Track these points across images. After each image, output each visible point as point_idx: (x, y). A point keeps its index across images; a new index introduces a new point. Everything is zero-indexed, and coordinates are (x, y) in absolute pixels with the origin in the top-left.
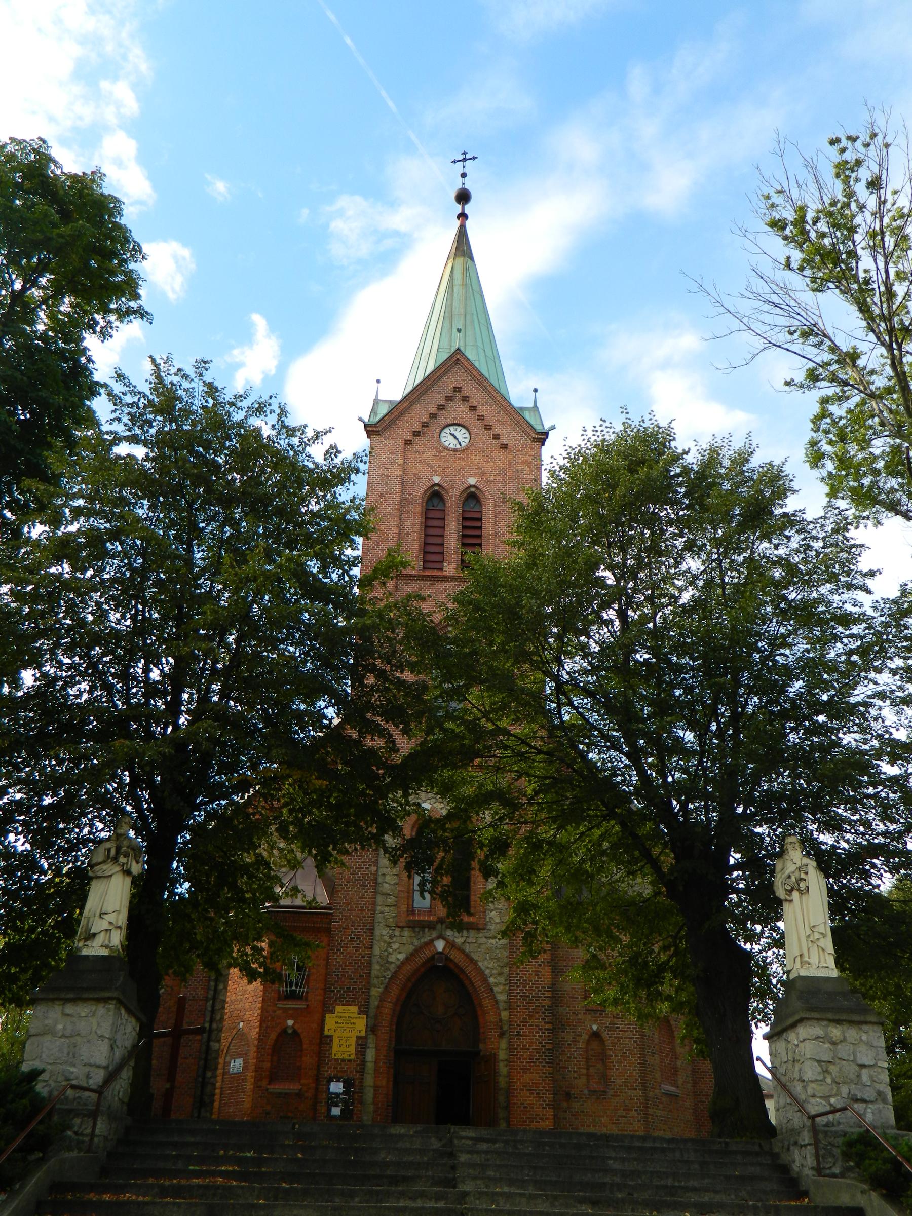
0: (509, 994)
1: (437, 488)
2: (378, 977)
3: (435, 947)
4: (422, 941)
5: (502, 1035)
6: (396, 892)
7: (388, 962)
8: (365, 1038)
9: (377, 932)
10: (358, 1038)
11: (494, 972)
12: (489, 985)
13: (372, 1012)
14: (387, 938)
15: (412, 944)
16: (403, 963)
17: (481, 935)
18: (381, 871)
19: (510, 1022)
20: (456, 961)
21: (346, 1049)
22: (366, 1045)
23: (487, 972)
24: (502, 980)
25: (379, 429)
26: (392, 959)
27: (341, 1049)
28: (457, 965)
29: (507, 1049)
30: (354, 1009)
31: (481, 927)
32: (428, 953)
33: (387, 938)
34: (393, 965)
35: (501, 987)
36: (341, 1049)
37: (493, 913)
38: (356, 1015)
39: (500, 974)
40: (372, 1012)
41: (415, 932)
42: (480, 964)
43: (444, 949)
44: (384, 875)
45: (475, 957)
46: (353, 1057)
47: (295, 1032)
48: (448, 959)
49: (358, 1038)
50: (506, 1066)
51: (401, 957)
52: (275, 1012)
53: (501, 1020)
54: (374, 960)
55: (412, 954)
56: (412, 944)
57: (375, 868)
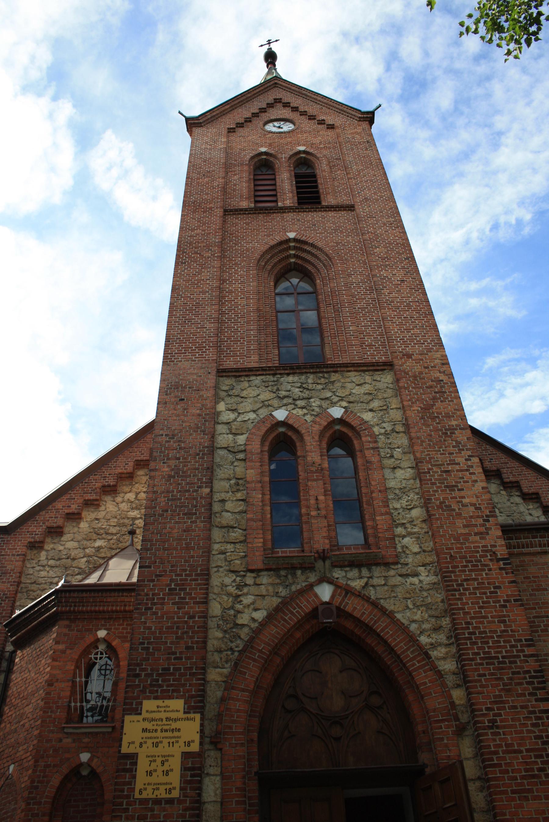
0: (460, 658)
1: (282, 430)
2: (220, 651)
3: (316, 596)
4: (294, 588)
5: (460, 731)
6: (244, 522)
7: (236, 625)
8: (200, 755)
9: (215, 581)
10: (186, 755)
11: (426, 626)
12: (420, 647)
13: (211, 709)
14: (232, 590)
15: (277, 594)
16: (263, 624)
17: (392, 573)
18: (217, 497)
19: (471, 705)
20: (357, 614)
21: (165, 779)
22: (200, 769)
23: (413, 627)
24: (442, 637)
25: (201, 121)
26: (243, 619)
27: (154, 779)
28: (357, 621)
29: (476, 756)
30: (178, 704)
31: (391, 560)
32: (306, 606)
33: (232, 590)
34: (246, 630)
35: (443, 650)
36: (154, 779)
37: (407, 540)
38: (181, 715)
39: (437, 629)
40: (211, 709)
41: (279, 576)
42: (399, 616)
43: (333, 597)
44: (223, 501)
45: (389, 605)
46: (176, 794)
47: (93, 772)
48: (341, 612)
49: (186, 755)
50: (481, 789)
51: (259, 615)
52: (61, 740)
53: (453, 704)
54: (212, 623)
55: (277, 609)
56: (277, 594)
57: (207, 490)
